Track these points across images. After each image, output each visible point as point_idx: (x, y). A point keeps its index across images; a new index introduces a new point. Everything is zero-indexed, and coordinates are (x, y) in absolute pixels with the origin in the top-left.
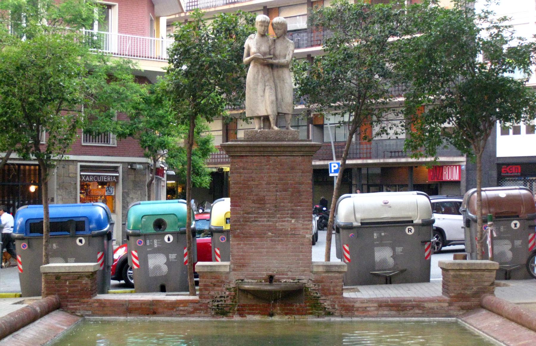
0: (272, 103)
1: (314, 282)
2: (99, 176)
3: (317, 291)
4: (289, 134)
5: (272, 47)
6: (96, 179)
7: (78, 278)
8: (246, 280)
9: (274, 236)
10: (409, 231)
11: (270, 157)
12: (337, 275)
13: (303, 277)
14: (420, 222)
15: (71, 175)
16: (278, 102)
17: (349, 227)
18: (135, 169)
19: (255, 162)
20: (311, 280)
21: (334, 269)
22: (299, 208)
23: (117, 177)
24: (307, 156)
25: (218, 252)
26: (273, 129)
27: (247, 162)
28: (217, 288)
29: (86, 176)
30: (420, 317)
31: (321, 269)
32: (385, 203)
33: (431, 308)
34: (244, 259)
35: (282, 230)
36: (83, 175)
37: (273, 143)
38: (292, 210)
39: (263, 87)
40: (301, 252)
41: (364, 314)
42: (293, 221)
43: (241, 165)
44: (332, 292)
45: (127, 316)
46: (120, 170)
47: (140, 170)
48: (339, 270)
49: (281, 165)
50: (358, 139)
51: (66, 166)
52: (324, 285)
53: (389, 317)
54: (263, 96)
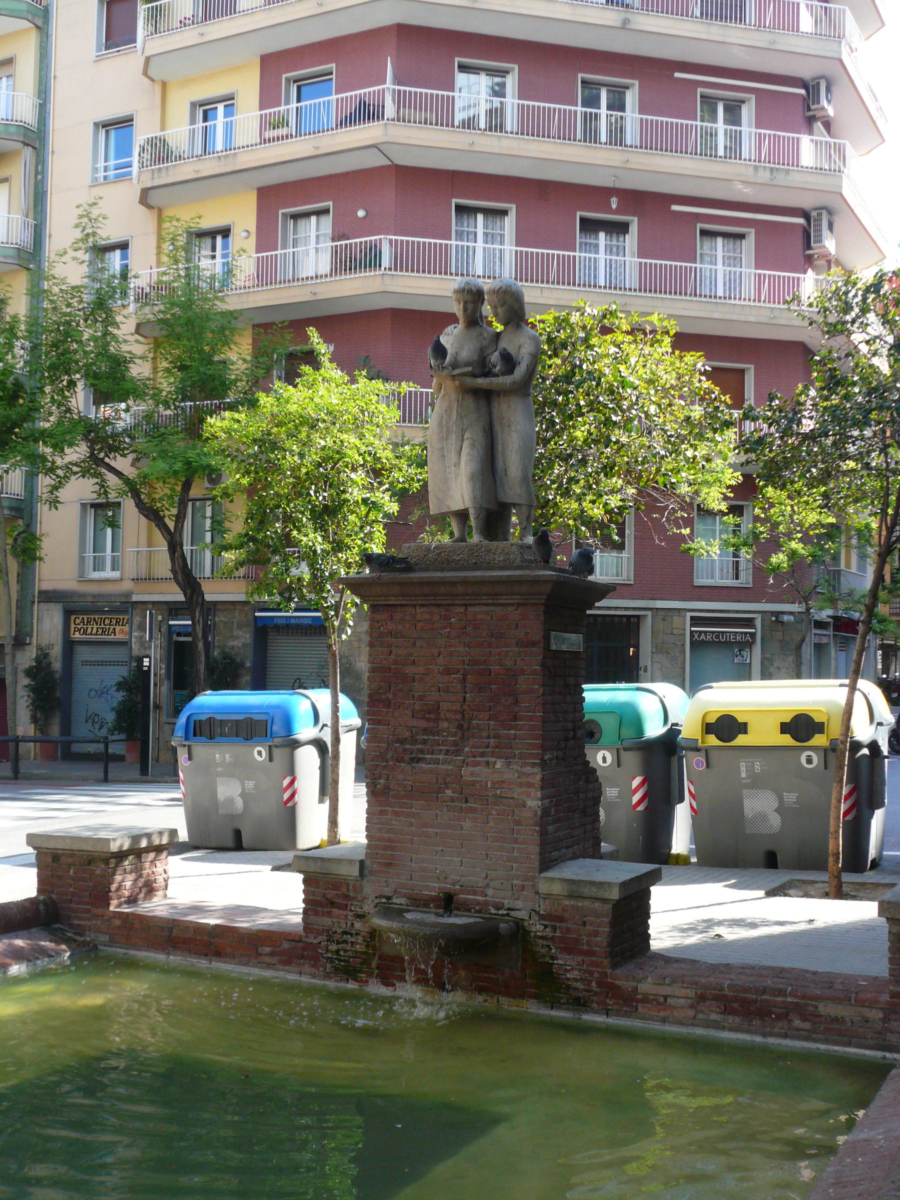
1: (542, 917)
2: (723, 633)
4: (499, 551)
6: (717, 637)
7: (90, 863)
11: (452, 608)
13: (519, 904)
15: (675, 632)
18: (783, 623)
20: (538, 913)
21: (586, 891)
23: (753, 635)
24: (533, 605)
28: (336, 911)
29: (701, 632)
30: (806, 1039)
33: (835, 1020)
34: (392, 848)
35: (473, 783)
36: (696, 632)
38: (497, 736)
40: (516, 841)
41: (662, 1014)
43: (391, 626)
44: (585, 947)
45: (168, 954)
46: (758, 623)
47: (789, 623)
48: (600, 894)
51: (667, 618)
53: (723, 1028)
54: (457, 465)
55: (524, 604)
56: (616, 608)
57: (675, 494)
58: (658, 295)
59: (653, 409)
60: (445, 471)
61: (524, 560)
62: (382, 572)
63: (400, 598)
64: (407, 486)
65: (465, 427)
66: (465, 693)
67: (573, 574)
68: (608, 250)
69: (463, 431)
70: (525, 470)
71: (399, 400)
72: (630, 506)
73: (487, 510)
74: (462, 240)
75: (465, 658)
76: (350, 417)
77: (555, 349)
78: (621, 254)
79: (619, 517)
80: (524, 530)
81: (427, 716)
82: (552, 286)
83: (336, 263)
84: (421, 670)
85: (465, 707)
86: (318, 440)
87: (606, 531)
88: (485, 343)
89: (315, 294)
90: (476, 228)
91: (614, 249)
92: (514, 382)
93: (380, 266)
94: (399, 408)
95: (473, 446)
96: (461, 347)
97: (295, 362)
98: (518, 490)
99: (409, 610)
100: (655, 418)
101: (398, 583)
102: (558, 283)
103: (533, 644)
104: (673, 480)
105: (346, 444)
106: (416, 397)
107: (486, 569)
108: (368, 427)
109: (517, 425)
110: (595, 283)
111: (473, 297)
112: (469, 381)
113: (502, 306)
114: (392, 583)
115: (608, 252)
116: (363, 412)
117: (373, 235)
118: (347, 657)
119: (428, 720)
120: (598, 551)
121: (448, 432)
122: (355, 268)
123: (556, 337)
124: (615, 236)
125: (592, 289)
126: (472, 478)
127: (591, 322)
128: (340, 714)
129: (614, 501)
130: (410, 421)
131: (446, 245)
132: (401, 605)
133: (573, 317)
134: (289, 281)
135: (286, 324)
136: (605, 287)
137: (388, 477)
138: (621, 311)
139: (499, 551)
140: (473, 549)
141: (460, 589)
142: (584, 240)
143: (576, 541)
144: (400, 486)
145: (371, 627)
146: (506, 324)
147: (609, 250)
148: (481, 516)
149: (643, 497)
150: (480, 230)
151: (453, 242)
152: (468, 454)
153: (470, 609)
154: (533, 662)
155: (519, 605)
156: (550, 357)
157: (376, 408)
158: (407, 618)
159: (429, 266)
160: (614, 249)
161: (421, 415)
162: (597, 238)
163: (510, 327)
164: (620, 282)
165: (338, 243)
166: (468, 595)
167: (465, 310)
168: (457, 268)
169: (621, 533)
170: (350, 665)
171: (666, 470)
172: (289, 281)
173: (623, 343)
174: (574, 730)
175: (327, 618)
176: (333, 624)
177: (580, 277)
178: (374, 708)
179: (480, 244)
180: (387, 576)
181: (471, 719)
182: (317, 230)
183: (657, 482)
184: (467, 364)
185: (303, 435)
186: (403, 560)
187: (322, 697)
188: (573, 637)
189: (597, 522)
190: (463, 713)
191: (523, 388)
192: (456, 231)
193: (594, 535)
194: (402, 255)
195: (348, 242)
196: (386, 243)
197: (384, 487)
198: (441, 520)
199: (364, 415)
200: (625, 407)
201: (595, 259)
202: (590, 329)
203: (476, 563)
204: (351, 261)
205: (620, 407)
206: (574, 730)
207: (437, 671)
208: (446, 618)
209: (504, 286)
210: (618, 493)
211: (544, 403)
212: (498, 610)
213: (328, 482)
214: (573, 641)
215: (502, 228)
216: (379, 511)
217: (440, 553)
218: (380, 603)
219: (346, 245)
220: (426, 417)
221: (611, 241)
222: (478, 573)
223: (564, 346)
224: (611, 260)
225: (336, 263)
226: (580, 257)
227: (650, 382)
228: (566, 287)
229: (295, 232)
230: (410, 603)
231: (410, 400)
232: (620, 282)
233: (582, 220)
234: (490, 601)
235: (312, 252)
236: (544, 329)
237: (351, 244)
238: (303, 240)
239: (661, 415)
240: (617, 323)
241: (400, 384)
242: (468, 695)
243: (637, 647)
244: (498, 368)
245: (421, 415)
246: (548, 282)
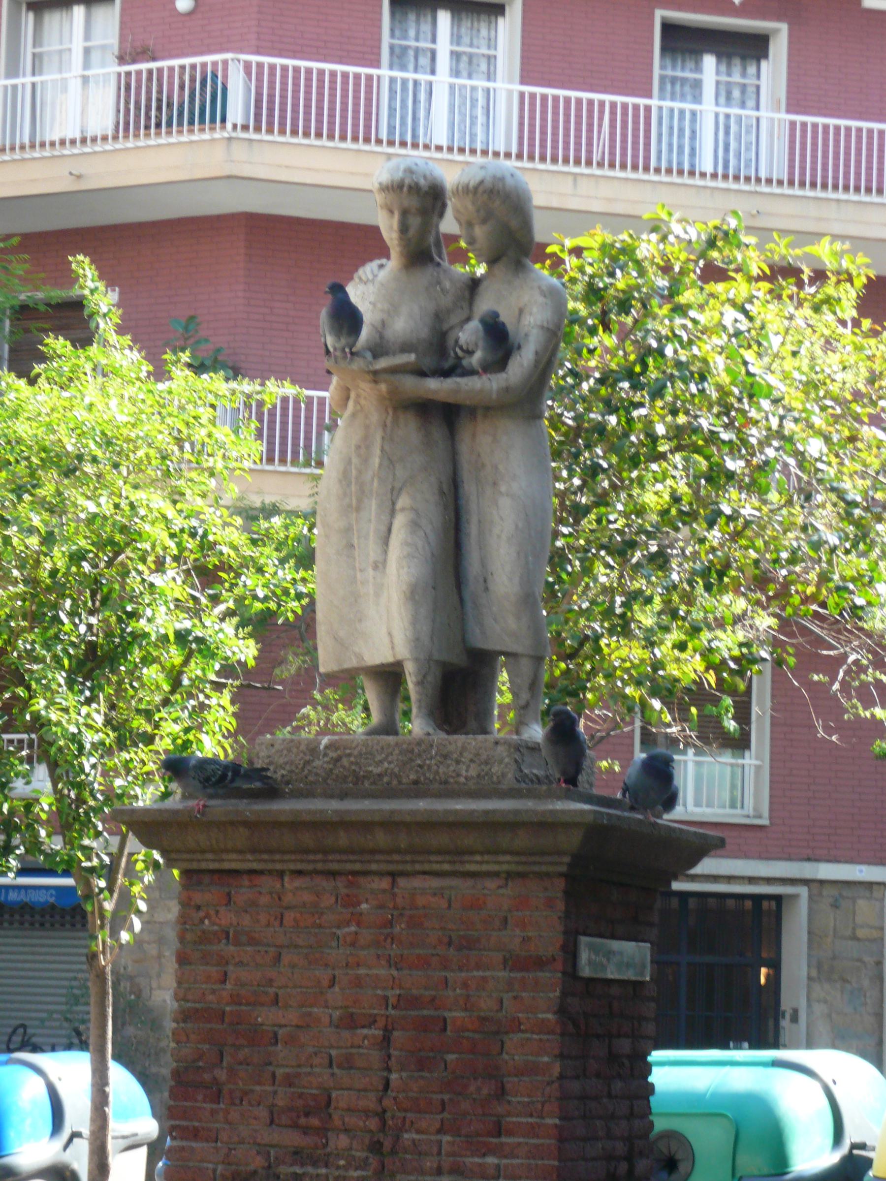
4: (467, 755)
11: (362, 880)
39: (385, 518)
43: (227, 918)
54: (380, 565)
55: (522, 875)
56: (730, 879)
57: (861, 629)
58: (830, 194)
59: (815, 447)
60: (353, 580)
61: (522, 778)
62: (211, 797)
63: (249, 857)
64: (273, 606)
65: (398, 485)
66: (389, 1070)
67: (632, 809)
68: (723, 93)
69: (394, 493)
70: (528, 578)
71: (260, 420)
72: (764, 660)
73: (444, 665)
74: (403, 68)
75: (389, 993)
76: (152, 453)
77: (605, 313)
78: (751, 103)
79: (738, 680)
80: (523, 709)
81: (303, 1121)
82: (599, 172)
83: (127, 111)
84: (292, 1016)
85: (386, 1102)
86: (81, 501)
87: (711, 709)
88: (446, 301)
89: (79, 177)
90: (434, 41)
91: (736, 93)
92: (507, 389)
93: (224, 120)
94: (259, 436)
95: (414, 525)
96: (393, 310)
97: (33, 325)
98: (512, 623)
99: (268, 883)
100: (819, 465)
101: (246, 824)
102: (612, 165)
103: (540, 963)
104: (860, 601)
105: (142, 512)
106: (297, 409)
107: (439, 795)
108: (193, 475)
109: (511, 482)
110: (692, 165)
111: (422, 199)
112: (411, 385)
113: (484, 221)
114: (232, 823)
115: (722, 100)
116: (179, 442)
117: (210, 52)
118: (131, 978)
119: (306, 1130)
120: (691, 752)
121: (362, 492)
122: (169, 124)
123: (605, 288)
124: (737, 61)
125: (686, 179)
126: (413, 594)
127: (683, 256)
128: (110, 1111)
129: (727, 643)
130: (283, 461)
131: (369, 78)
132: (252, 872)
133: (644, 245)
134: (22, 147)
135: (15, 241)
136: (714, 176)
137: (233, 585)
138: (750, 230)
139: (467, 755)
140: (414, 751)
141: (381, 839)
142: (669, 72)
143: (643, 729)
144: (258, 606)
145: (183, 919)
146: (492, 262)
147: (725, 93)
148: (430, 678)
149: (791, 635)
150: (444, 46)
151: (385, 72)
152: (406, 543)
153: (402, 882)
154: (542, 1000)
155: (510, 876)
156: (593, 331)
157: (210, 436)
158: (264, 900)
159: (332, 123)
160: (736, 93)
161: (308, 447)
162: (698, 69)
163: (499, 269)
164: (748, 166)
165: (133, 68)
166: (398, 851)
167: (404, 229)
168: (391, 129)
169: (743, 715)
170: (138, 996)
171: (843, 578)
172: (22, 147)
173: (750, 300)
174: (629, 1158)
175: (89, 895)
176: (101, 908)
177: (660, 152)
178: (183, 1098)
179: (443, 77)
180: (220, 807)
181: (401, 1129)
182: (87, 36)
183: (823, 605)
184: (405, 348)
185: (47, 491)
186: (258, 774)
187: (70, 1070)
188: (628, 948)
189: (688, 690)
190: (382, 1115)
191: (526, 402)
192: (392, 48)
193: (683, 716)
194: (271, 97)
195: (153, 65)
196: (238, 73)
197: (222, 608)
198: (346, 682)
199: (181, 448)
200: (753, 441)
201: (694, 114)
202: (682, 272)
203: (416, 782)
204: (159, 108)
205: (744, 442)
206: (629, 1158)
207: (325, 1020)
208: (351, 902)
209: (489, 179)
210: (740, 625)
211: (577, 431)
212: (464, 886)
213: (100, 595)
214: (626, 958)
215: (492, 43)
216: (213, 656)
217: (338, 760)
218: (204, 866)
219: (150, 72)
220: (320, 451)
221: (729, 74)
222: (422, 804)
223: (624, 306)
224: (728, 116)
225: (127, 111)
226: (660, 108)
227: (810, 386)
228: (629, 174)
229: (37, 42)
230: (270, 866)
231: (284, 414)
232: (748, 166)
233: (669, 28)
234: (446, 867)
235: (75, 85)
236: (581, 270)
237: (160, 71)
238: (56, 58)
239: (834, 460)
240: (739, 257)
241: (263, 384)
242: (394, 1076)
243: (775, 966)
244: (478, 355)
245: (308, 447)
246: (589, 163)
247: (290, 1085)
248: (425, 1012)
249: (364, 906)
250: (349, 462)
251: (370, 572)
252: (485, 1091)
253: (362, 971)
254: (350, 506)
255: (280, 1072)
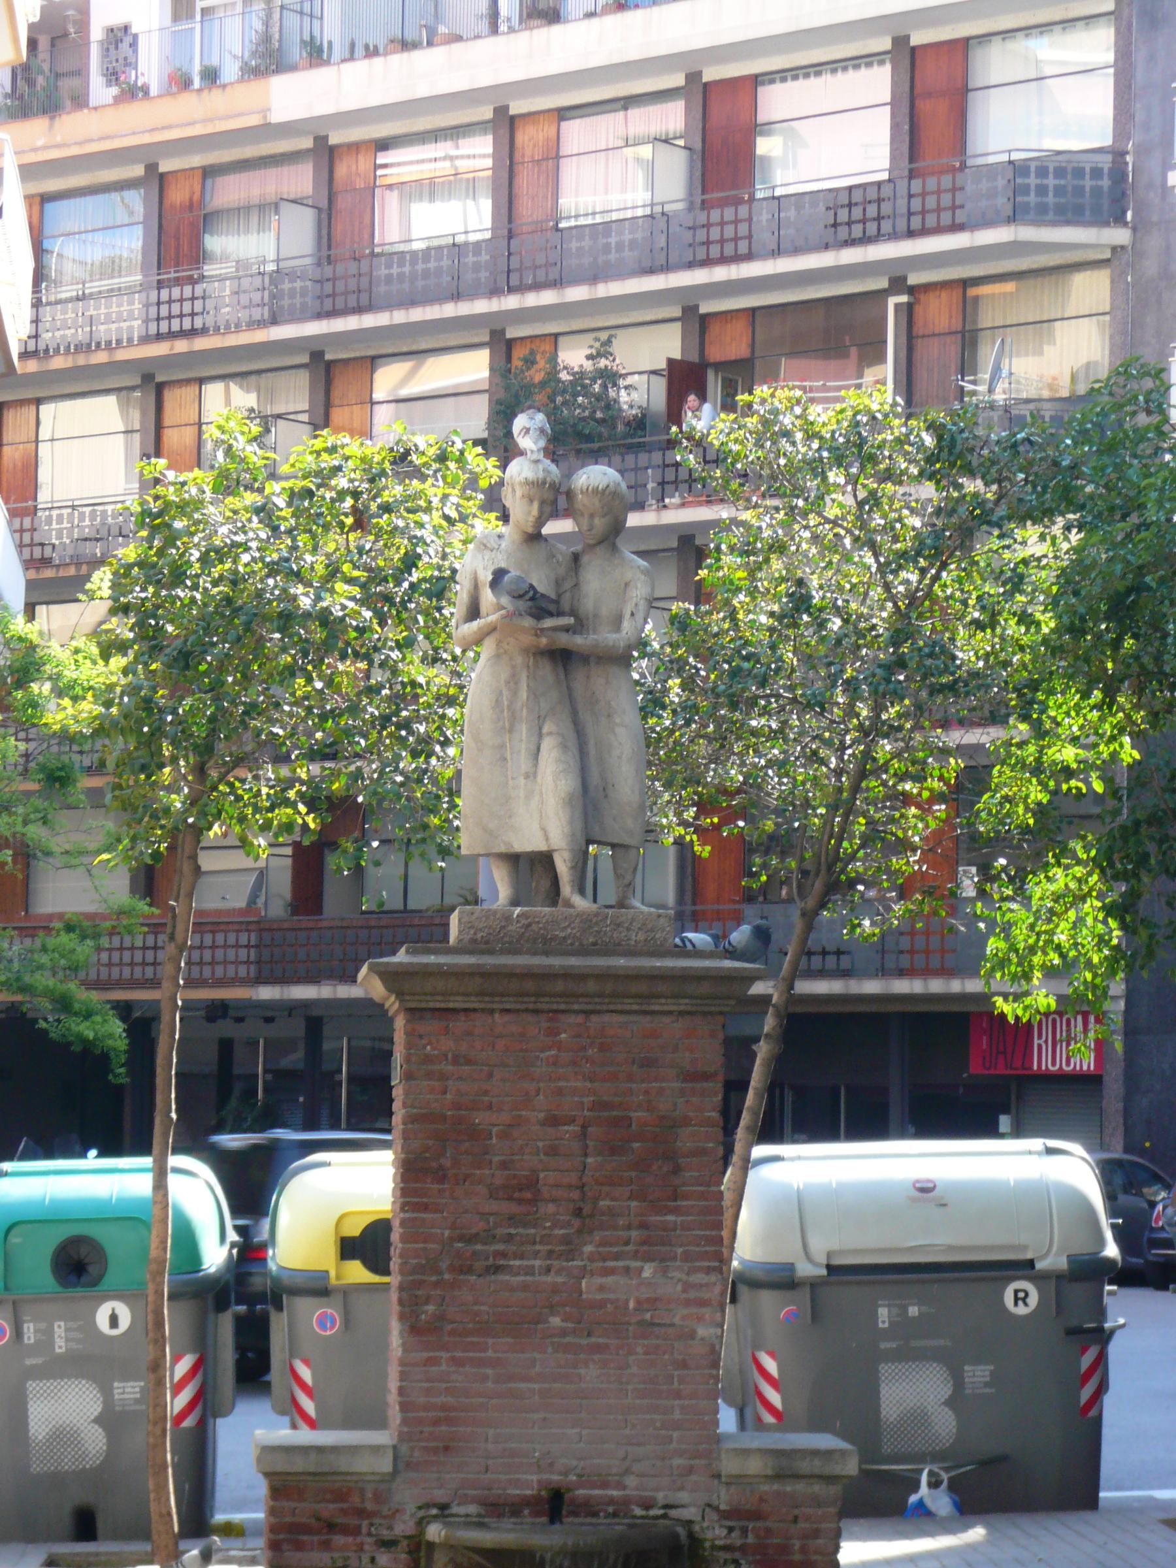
0: (570, 801)
1: (725, 1515)
3: (737, 1555)
4: (636, 925)
5: (567, 585)
8: (455, 1509)
9: (574, 1332)
10: (1016, 1299)
11: (561, 1017)
12: (817, 1488)
13: (684, 1497)
14: (1062, 1263)
16: (589, 801)
17: (782, 1280)
19: (500, 1036)
20: (716, 1509)
21: (805, 1467)
22: (671, 1218)
25: (306, 1374)
26: (568, 904)
27: (469, 1033)
31: (754, 1466)
32: (923, 1190)
34: (449, 1421)
35: (602, 1304)
37: (573, 961)
38: (643, 1226)
40: (678, 1395)
42: (647, 1273)
49: (603, 1048)
50: (688, 897)
52: (768, 1531)
54: (531, 775)
69: (540, 721)
75: (585, 1100)
81: (516, 1195)
84: (505, 1117)
103: (706, 1077)
119: (520, 1201)
121: (514, 718)
132: (466, 1010)
139: (636, 925)
153: (594, 1018)
181: (596, 1199)
203: (595, 944)
208: (553, 1032)
217: (529, 925)
234: (635, 1007)
242: (590, 1160)
247: (506, 1168)
248: (615, 1113)
249: (563, 1035)
250: (501, 693)
251: (522, 781)
252: (665, 1169)
253: (562, 1084)
254: (503, 728)
255: (496, 1159)
